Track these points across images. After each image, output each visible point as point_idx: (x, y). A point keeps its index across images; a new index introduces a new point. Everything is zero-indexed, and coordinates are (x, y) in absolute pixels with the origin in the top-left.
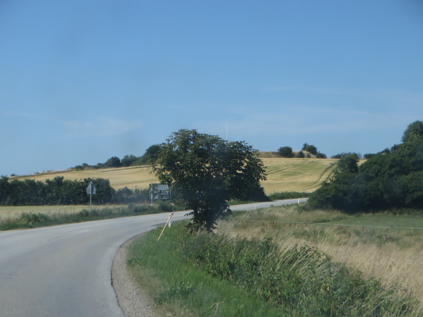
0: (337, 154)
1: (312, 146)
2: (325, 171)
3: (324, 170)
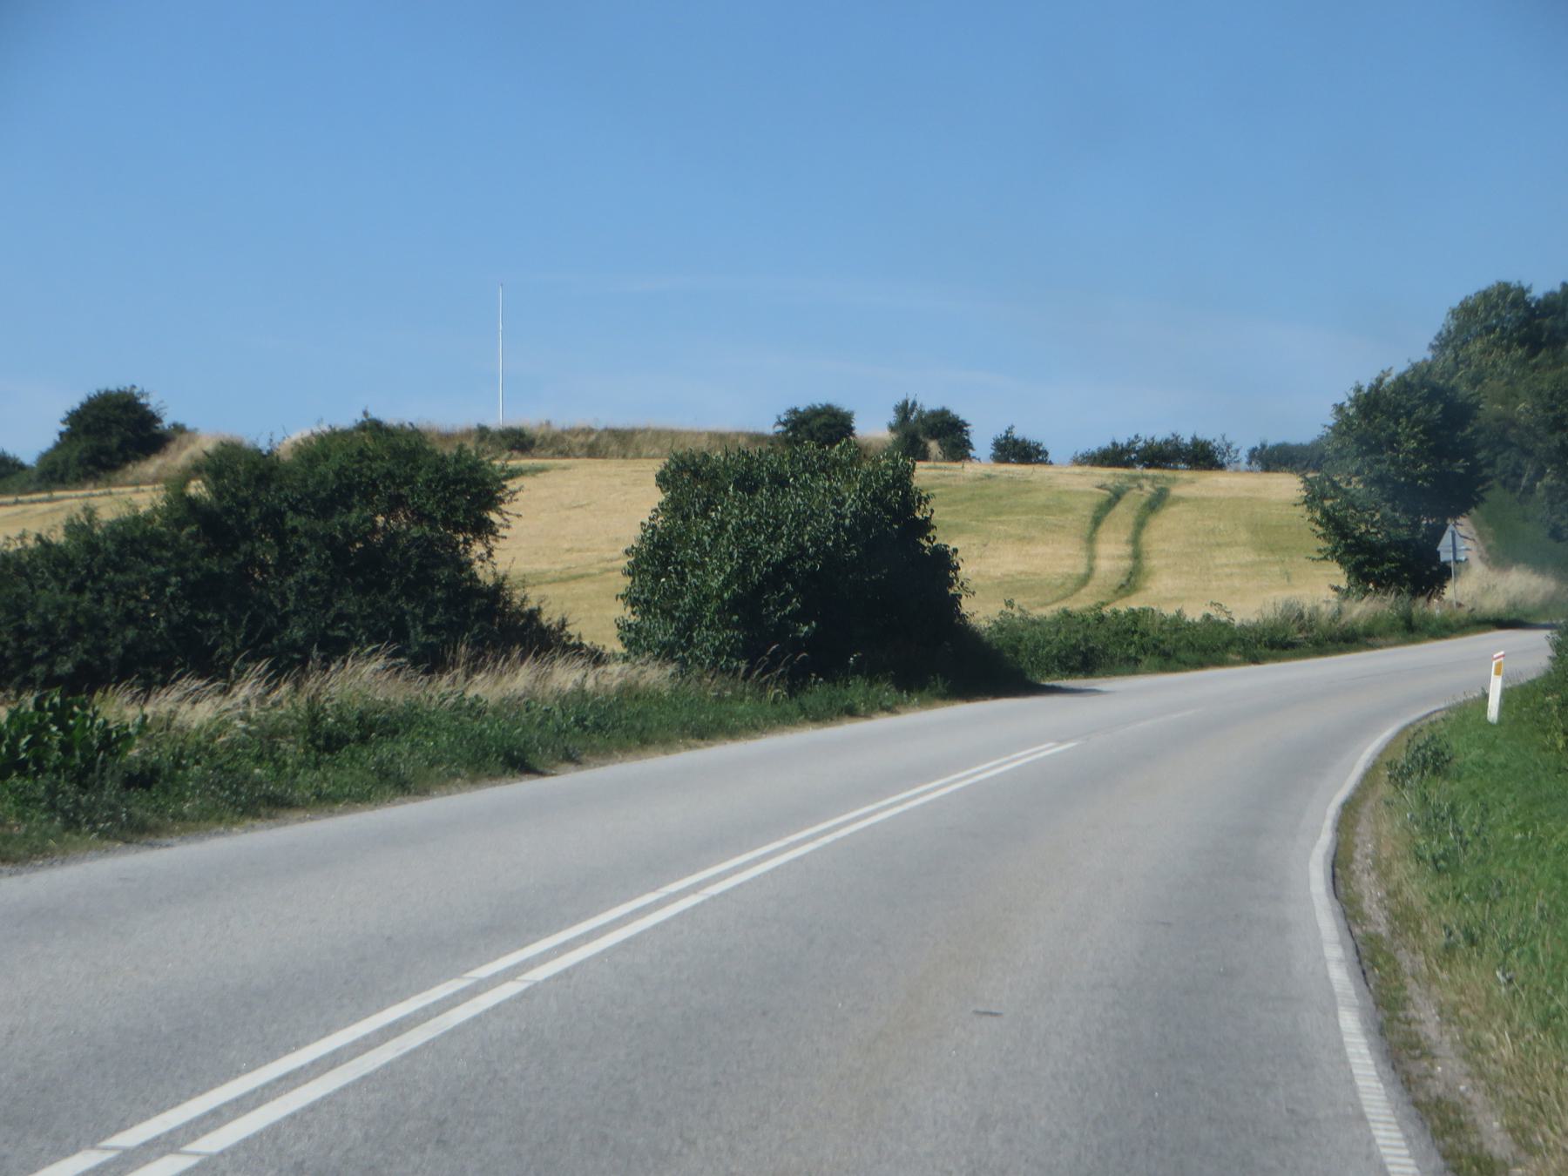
0: (1106, 444)
1: (943, 414)
2: (1097, 522)
3: (1088, 513)
